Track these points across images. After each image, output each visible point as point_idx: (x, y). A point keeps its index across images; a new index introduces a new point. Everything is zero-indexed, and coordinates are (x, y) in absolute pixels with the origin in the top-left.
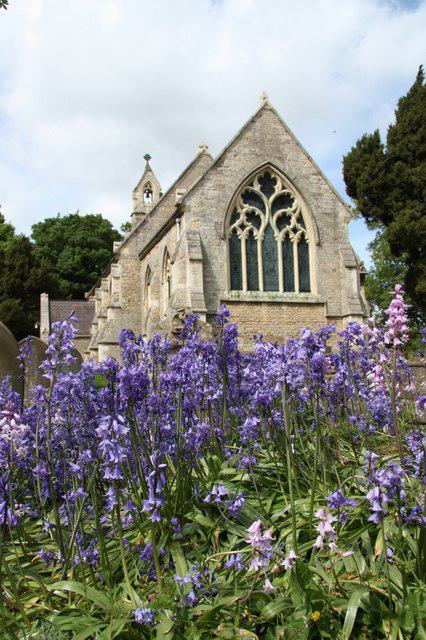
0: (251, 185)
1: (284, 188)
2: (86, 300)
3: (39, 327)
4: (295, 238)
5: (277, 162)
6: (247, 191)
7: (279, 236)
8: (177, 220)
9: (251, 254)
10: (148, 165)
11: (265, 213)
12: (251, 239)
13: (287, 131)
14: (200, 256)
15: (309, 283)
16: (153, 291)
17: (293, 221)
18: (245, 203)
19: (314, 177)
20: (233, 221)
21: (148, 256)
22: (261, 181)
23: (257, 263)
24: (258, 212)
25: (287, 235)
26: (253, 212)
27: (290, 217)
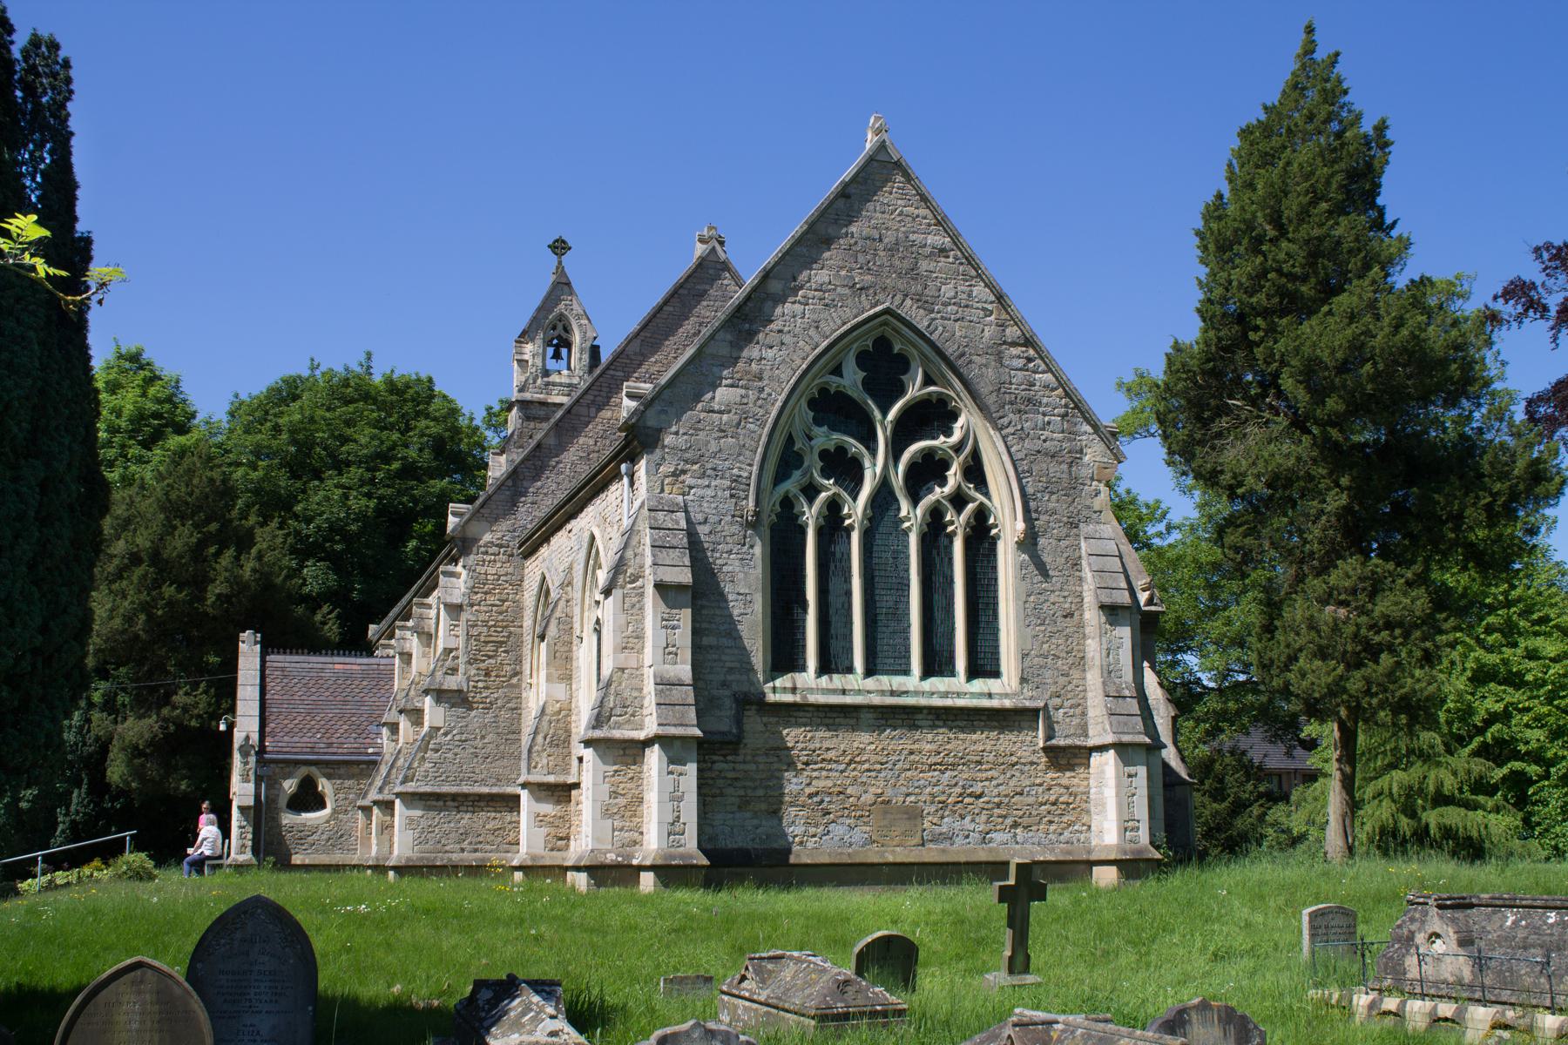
0: (837, 371)
1: (928, 381)
2: (367, 649)
3: (231, 726)
4: (958, 523)
5: (910, 310)
6: (823, 391)
7: (912, 516)
8: (623, 467)
9: (831, 564)
10: (560, 267)
11: (873, 452)
12: (833, 525)
13: (941, 223)
14: (685, 576)
15: (997, 647)
16: (553, 656)
17: (954, 476)
18: (818, 422)
19: (1015, 351)
20: (781, 476)
21: (544, 551)
22: (863, 359)
23: (849, 593)
24: (855, 446)
25: (936, 513)
26: (841, 450)
27: (946, 465)
